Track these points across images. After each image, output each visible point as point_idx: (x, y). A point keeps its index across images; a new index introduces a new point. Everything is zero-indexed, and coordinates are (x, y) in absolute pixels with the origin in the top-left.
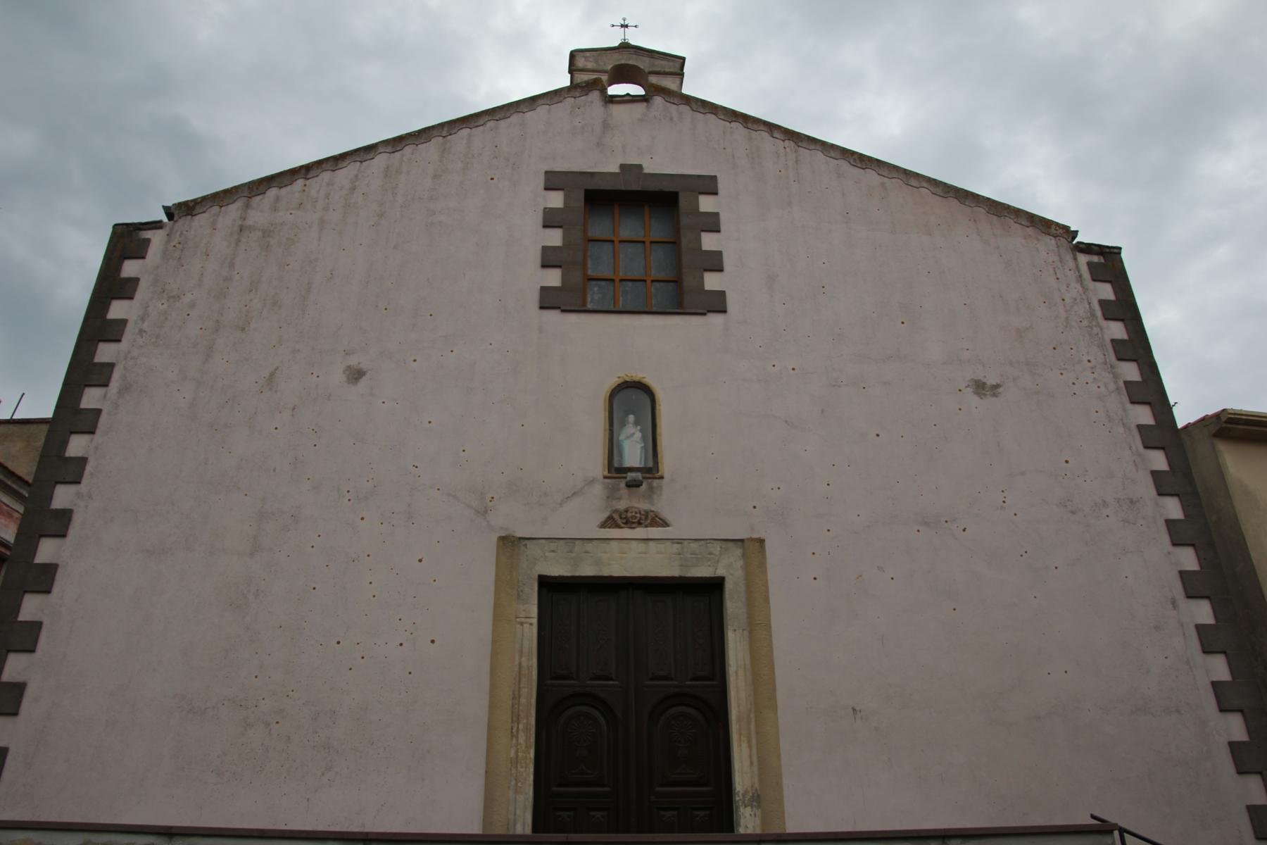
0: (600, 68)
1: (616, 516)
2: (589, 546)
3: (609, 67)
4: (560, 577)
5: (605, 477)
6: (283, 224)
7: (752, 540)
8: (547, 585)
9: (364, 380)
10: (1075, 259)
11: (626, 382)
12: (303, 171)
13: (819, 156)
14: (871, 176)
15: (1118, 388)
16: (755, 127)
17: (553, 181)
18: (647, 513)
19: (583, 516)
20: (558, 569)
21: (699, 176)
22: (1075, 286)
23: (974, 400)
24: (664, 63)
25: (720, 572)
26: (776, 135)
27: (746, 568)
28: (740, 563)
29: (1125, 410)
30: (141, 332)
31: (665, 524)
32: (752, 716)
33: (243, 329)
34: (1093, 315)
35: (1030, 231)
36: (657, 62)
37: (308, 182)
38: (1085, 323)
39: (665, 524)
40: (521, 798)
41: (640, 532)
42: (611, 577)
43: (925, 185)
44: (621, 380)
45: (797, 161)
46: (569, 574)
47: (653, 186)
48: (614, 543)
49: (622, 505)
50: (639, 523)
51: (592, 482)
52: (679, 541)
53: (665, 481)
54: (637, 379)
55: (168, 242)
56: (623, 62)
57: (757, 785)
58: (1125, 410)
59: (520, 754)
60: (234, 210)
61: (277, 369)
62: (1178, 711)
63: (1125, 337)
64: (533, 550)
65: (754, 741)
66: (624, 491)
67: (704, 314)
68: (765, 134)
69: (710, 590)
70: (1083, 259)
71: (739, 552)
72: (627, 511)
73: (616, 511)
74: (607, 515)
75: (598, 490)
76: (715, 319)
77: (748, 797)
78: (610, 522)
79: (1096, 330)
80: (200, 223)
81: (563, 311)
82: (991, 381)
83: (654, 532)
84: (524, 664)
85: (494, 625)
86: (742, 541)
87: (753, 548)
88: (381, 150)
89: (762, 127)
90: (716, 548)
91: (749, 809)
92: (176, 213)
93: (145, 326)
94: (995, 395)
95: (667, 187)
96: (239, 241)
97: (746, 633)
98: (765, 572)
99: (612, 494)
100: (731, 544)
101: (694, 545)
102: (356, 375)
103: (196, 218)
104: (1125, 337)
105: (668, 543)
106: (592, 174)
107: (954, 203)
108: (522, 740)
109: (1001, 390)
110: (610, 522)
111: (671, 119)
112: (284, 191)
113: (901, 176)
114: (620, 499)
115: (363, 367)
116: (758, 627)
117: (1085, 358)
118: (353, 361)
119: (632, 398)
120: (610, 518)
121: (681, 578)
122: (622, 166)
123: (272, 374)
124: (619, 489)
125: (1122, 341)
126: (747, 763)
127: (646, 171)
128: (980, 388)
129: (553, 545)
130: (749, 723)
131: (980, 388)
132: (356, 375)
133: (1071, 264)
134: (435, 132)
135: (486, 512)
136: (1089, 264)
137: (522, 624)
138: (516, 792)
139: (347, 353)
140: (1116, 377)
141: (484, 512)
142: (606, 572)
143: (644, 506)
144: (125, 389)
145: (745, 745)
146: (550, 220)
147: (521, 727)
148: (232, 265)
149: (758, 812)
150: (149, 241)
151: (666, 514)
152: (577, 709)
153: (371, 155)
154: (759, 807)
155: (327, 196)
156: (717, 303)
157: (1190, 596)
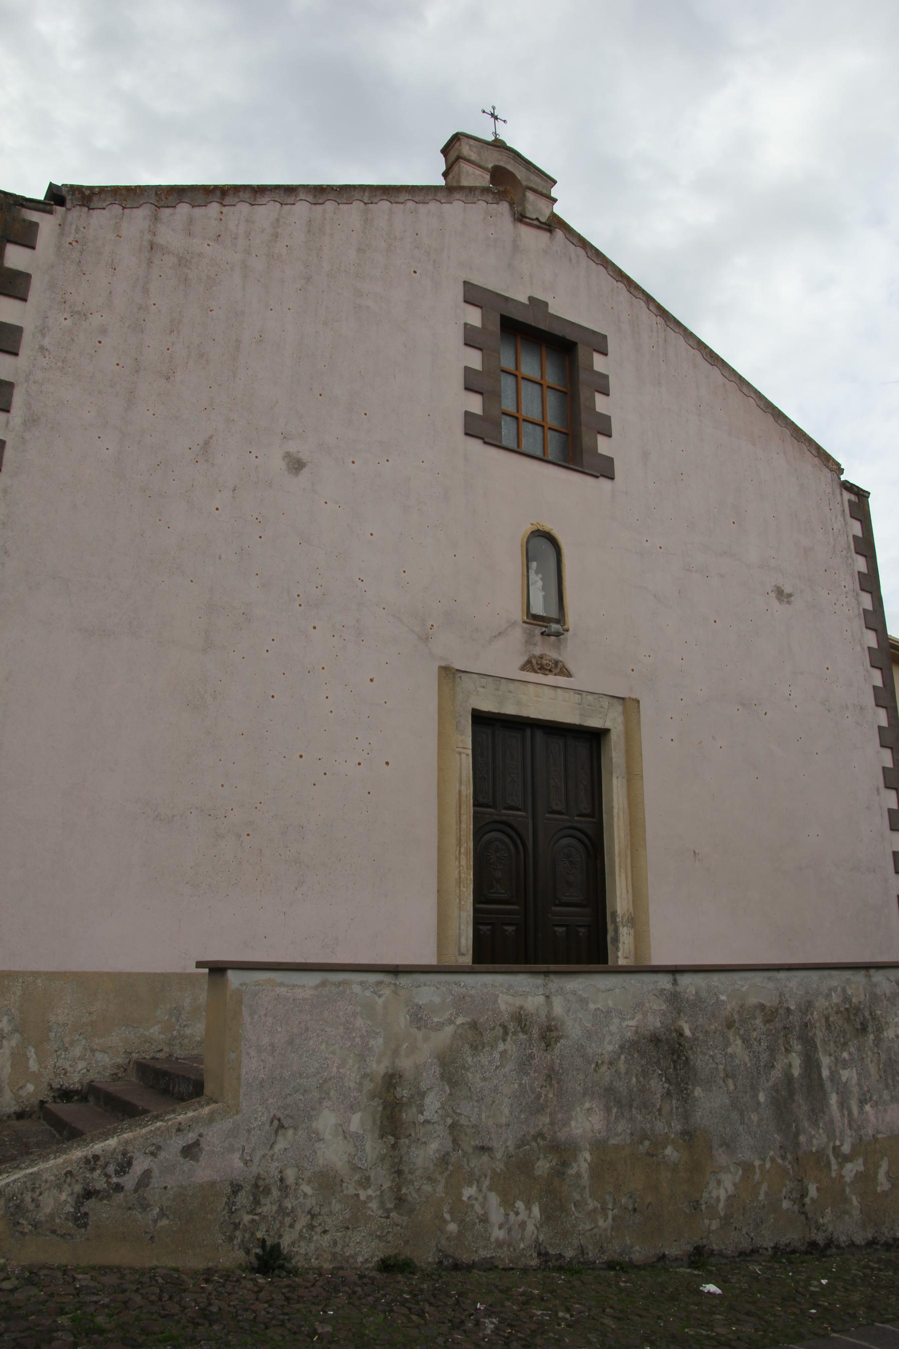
0: (482, 164)
1: (534, 662)
2: (512, 686)
3: (490, 166)
4: (489, 712)
5: (524, 622)
6: (200, 255)
7: (630, 698)
8: (480, 719)
9: (305, 472)
10: (841, 495)
11: (538, 530)
12: (218, 193)
13: (681, 341)
14: (716, 373)
15: (859, 614)
16: (636, 293)
17: (473, 295)
18: (556, 663)
19: (505, 655)
20: (488, 706)
21: (594, 332)
22: (840, 518)
23: (775, 603)
24: (538, 180)
25: (608, 725)
26: (652, 308)
27: (627, 723)
28: (620, 719)
29: (862, 633)
30: (42, 349)
31: (569, 675)
32: (629, 852)
33: (168, 378)
34: (849, 547)
35: (816, 460)
36: (533, 177)
37: (225, 210)
38: (844, 553)
39: (569, 675)
40: (464, 915)
41: (551, 679)
42: (528, 718)
43: (753, 395)
44: (535, 528)
45: (665, 340)
46: (497, 711)
47: (558, 330)
48: (531, 687)
49: (537, 651)
50: (550, 671)
51: (513, 624)
52: (579, 692)
53: (570, 633)
54: (547, 530)
55: (62, 234)
56: (502, 164)
57: (631, 910)
58: (862, 633)
59: (463, 875)
60: (140, 216)
61: (211, 437)
62: (874, 871)
63: (866, 572)
64: (466, 683)
65: (629, 874)
66: (538, 638)
67: (597, 477)
68: (643, 304)
69: (596, 737)
70: (847, 496)
71: (620, 708)
72: (541, 657)
73: (534, 656)
74: (526, 658)
75: (518, 634)
76: (604, 483)
77: (625, 919)
78: (528, 666)
79: (850, 561)
80: (100, 219)
81: (485, 443)
82: (787, 590)
83: (561, 681)
84: (464, 793)
85: (439, 753)
86: (623, 699)
87: (629, 705)
88: (302, 196)
89: (641, 296)
90: (605, 702)
91: (625, 928)
92: (68, 198)
93: (46, 342)
94: (789, 603)
95: (571, 336)
96: (150, 262)
97: (624, 780)
98: (640, 729)
99: (529, 641)
100: (615, 700)
101: (590, 698)
102: (296, 465)
103: (95, 213)
104: (866, 572)
105: (572, 692)
106: (507, 299)
107: (770, 419)
108: (463, 863)
109: (792, 599)
110: (528, 666)
111: (570, 260)
112: (198, 212)
113: (738, 382)
114: (535, 645)
115: (304, 456)
116: (633, 777)
117: (843, 584)
118: (293, 447)
119: (543, 546)
120: (529, 662)
121: (580, 726)
122: (531, 299)
123: (207, 443)
124: (534, 636)
125: (864, 574)
126: (624, 891)
127: (551, 311)
128: (781, 595)
129: (484, 681)
130: (626, 858)
131: (781, 595)
132: (296, 465)
133: (839, 497)
134: (357, 195)
135: (427, 639)
136: (849, 501)
137: (460, 753)
138: (460, 909)
139: (285, 437)
140: (859, 603)
141: (426, 639)
142: (525, 713)
143: (554, 655)
144: (32, 421)
145: (623, 876)
146: (472, 338)
147: (462, 850)
148: (146, 291)
149: (632, 931)
150: (35, 226)
151: (571, 666)
152: (493, 834)
153: (291, 200)
154: (632, 927)
155: (248, 235)
156: (604, 469)
157: (887, 787)
